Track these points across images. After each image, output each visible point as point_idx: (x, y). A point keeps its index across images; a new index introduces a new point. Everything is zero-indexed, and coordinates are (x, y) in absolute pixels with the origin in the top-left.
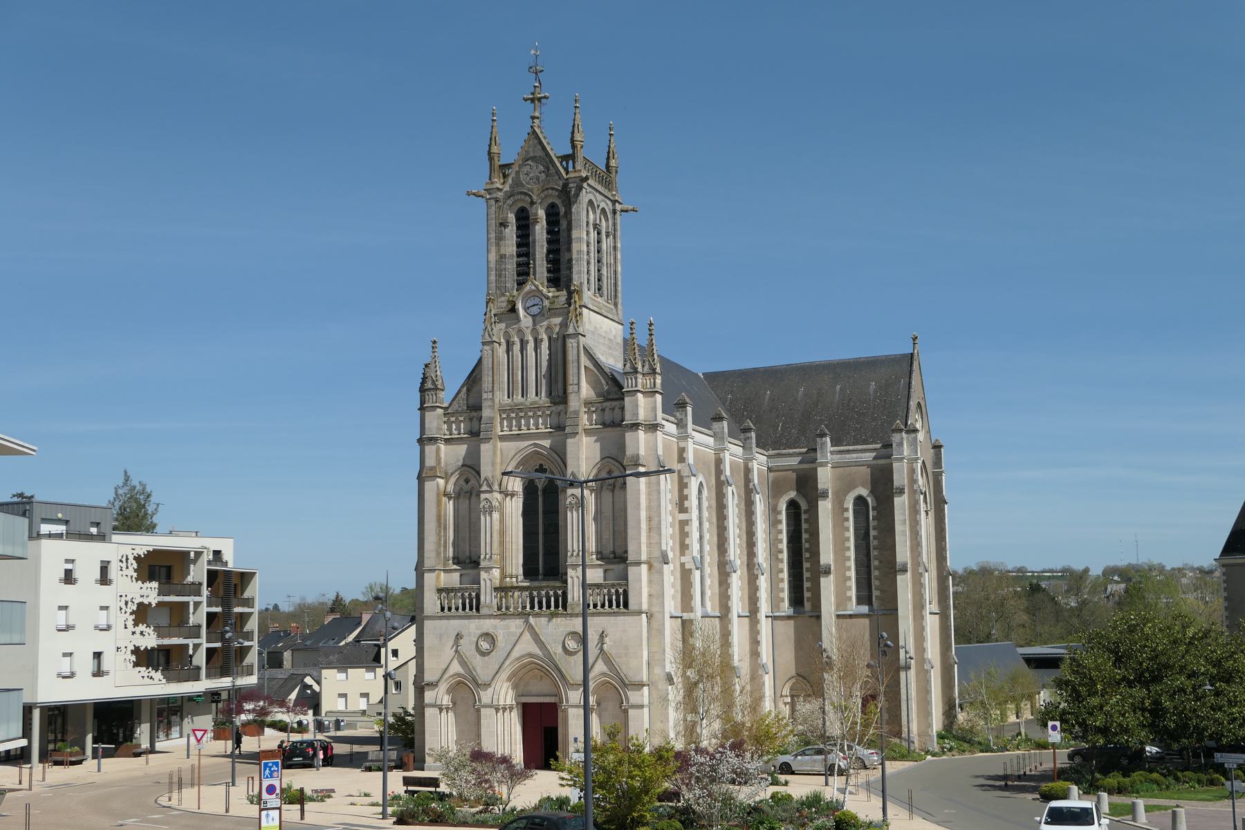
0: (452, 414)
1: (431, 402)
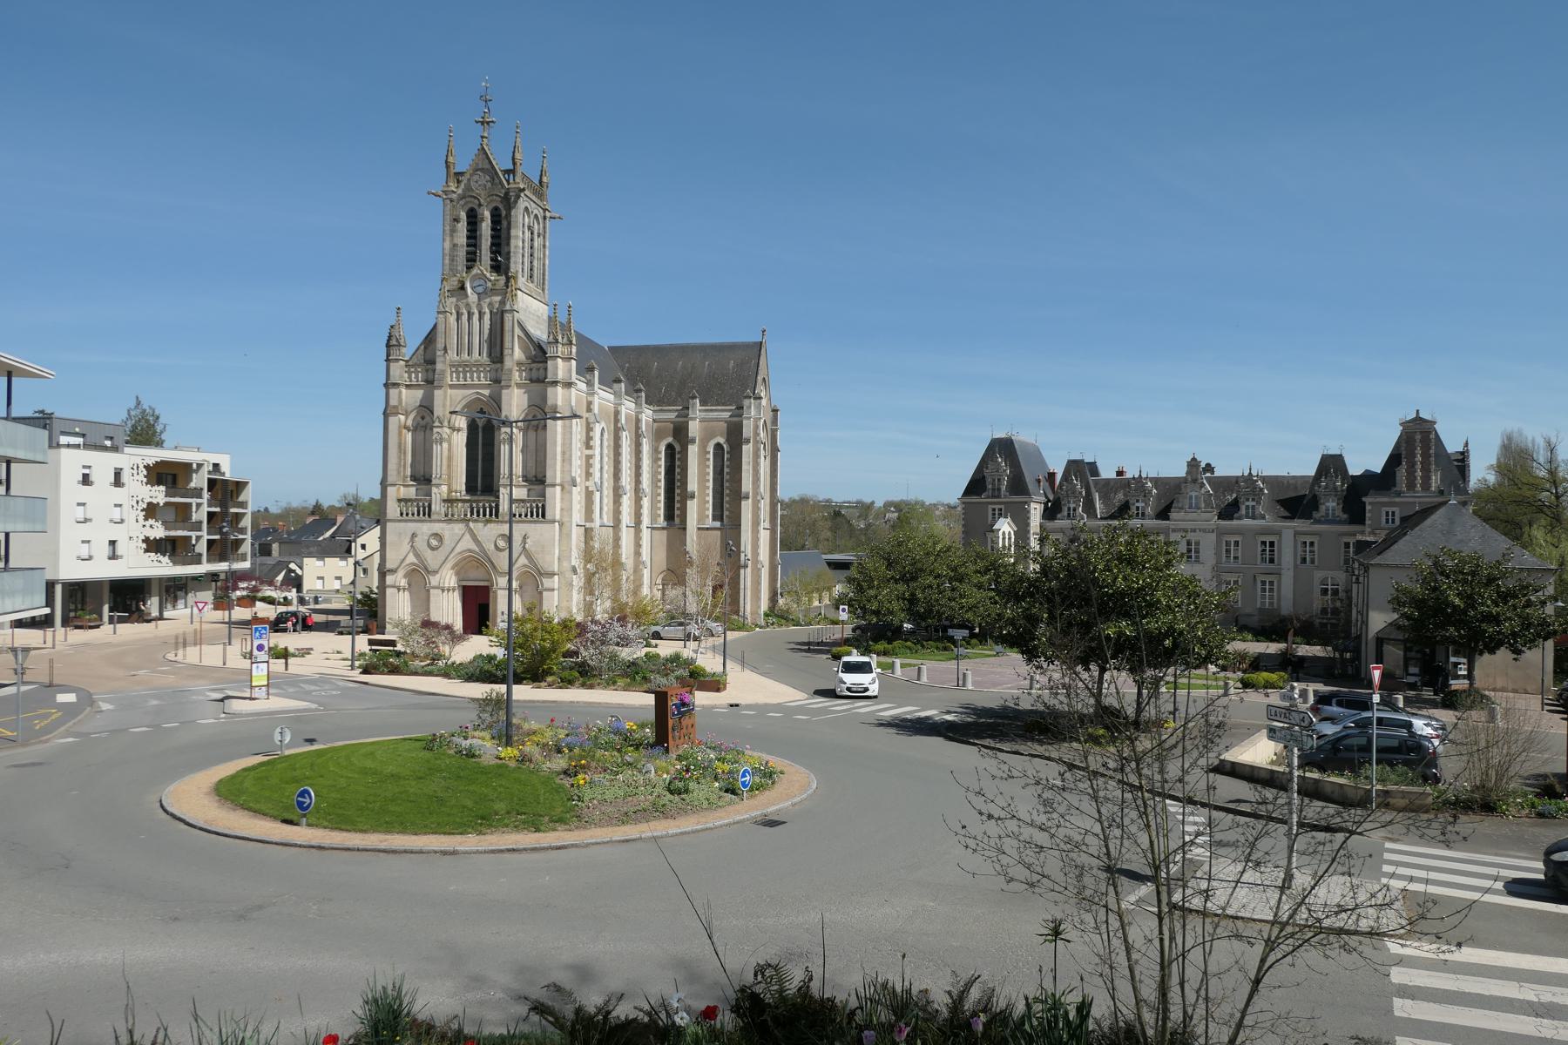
0: (413, 366)
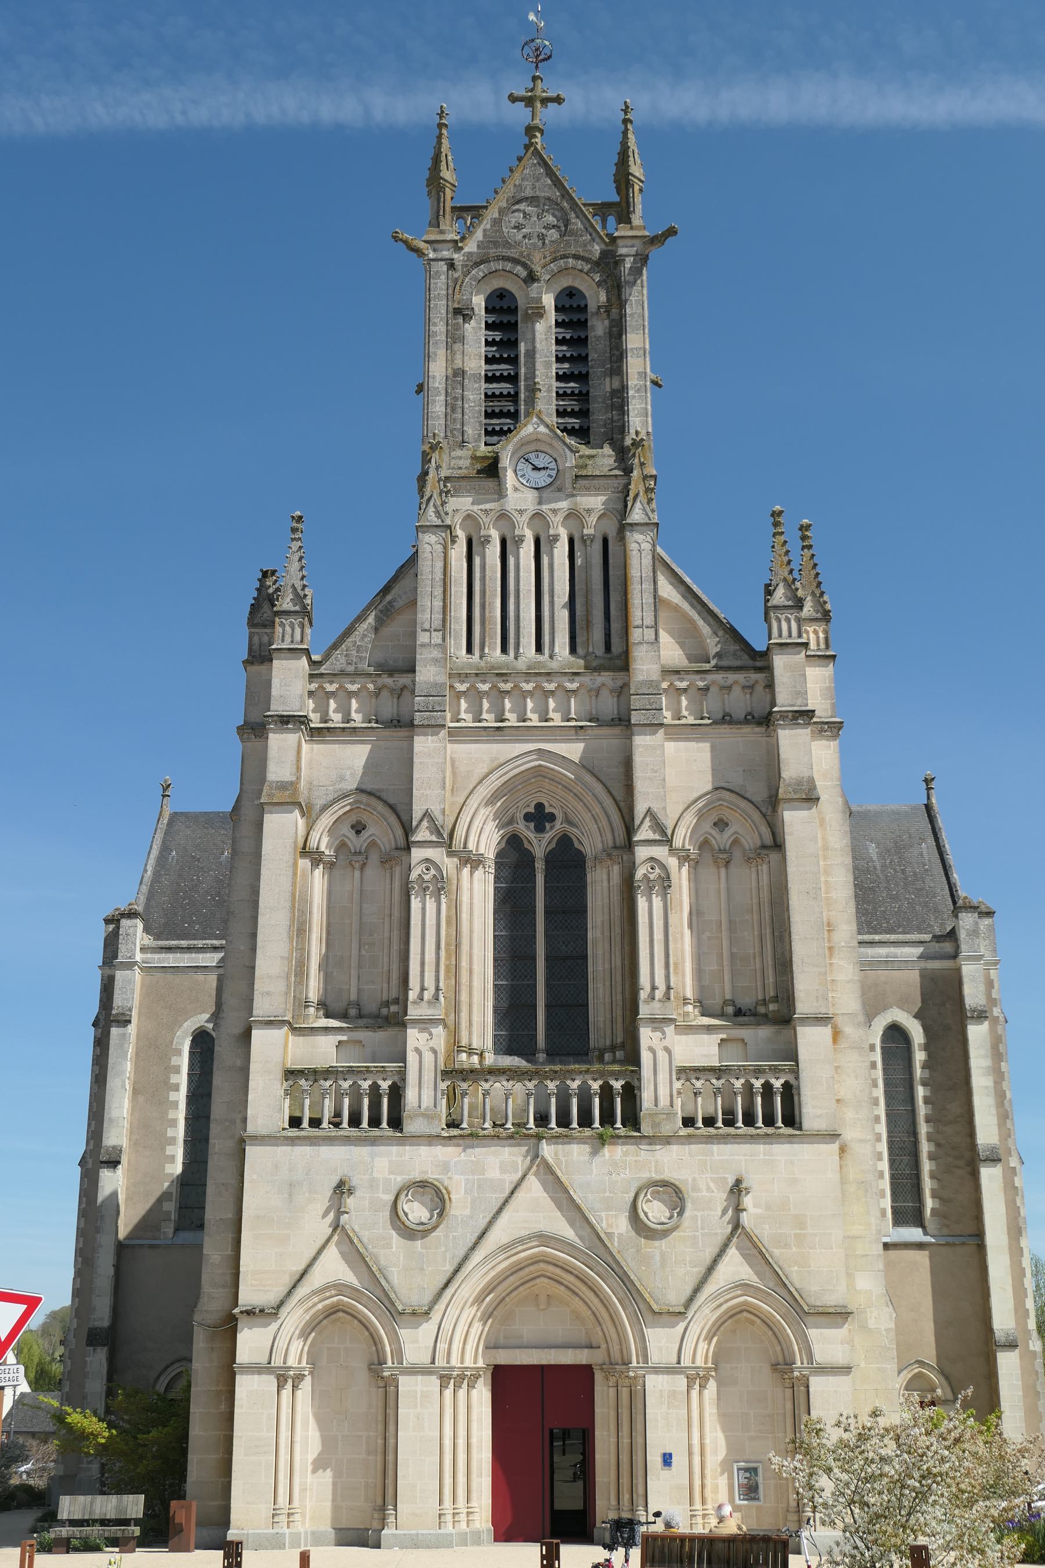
0: (333, 676)
1: (288, 638)
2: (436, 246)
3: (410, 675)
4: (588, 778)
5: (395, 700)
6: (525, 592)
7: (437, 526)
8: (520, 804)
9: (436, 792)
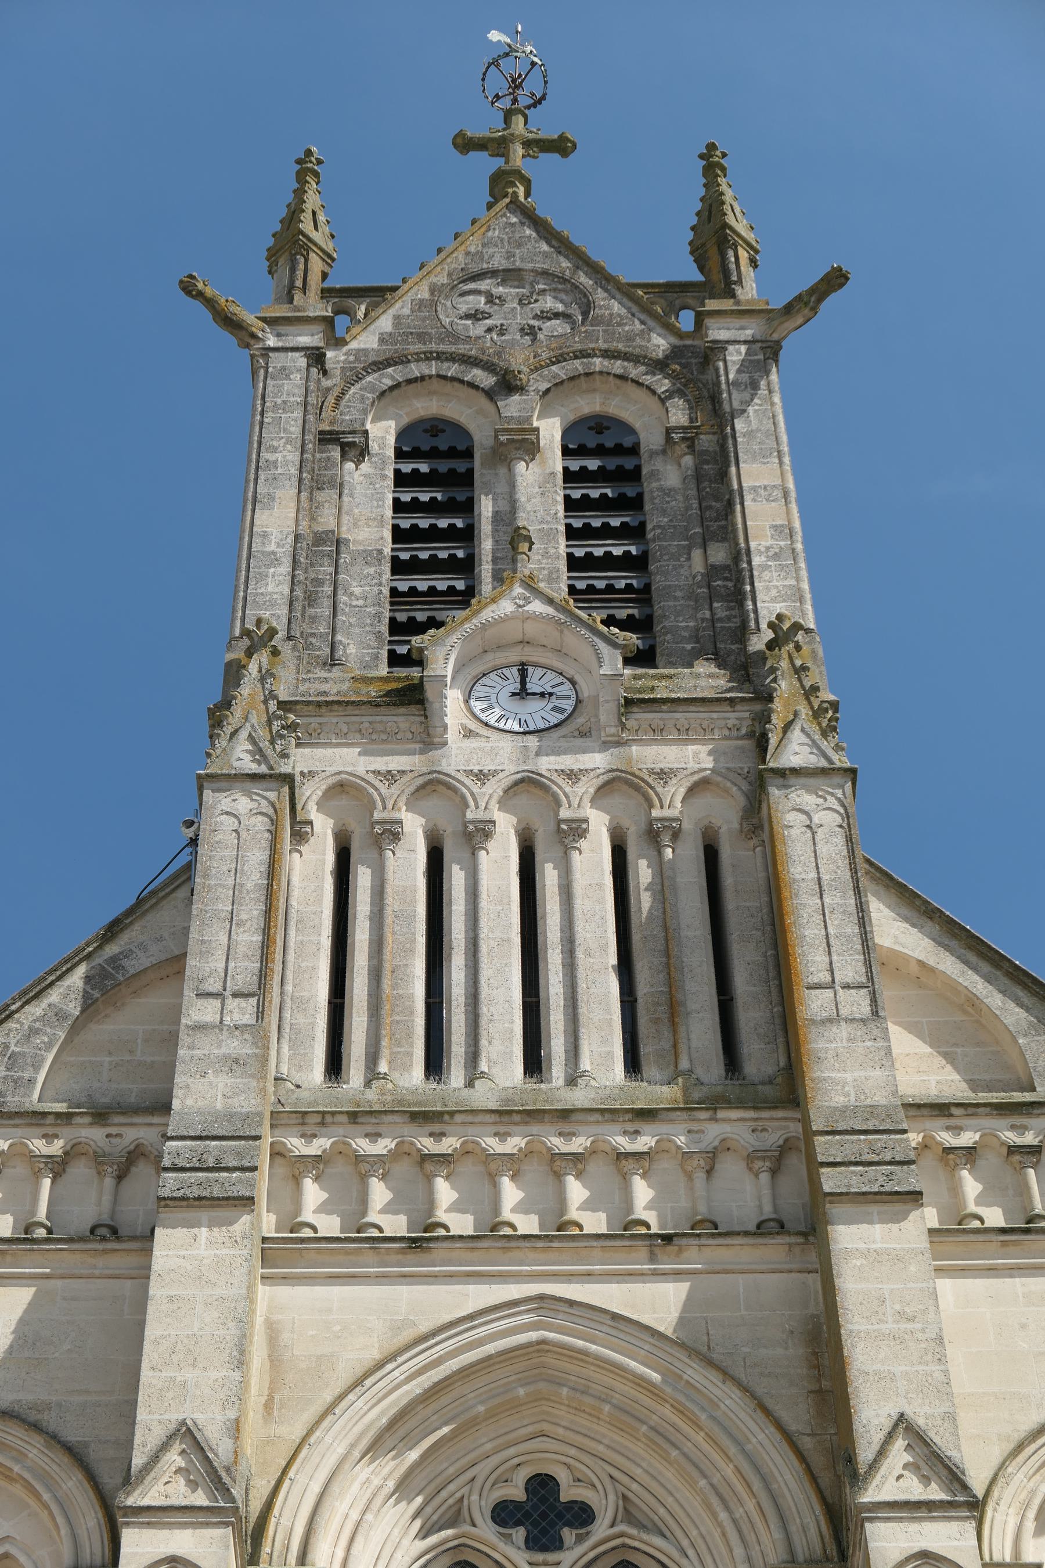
2: (282, 329)
3: (156, 1120)
4: (695, 1373)
5: (109, 1182)
6: (493, 944)
7: (254, 777)
8: (481, 1470)
9: (213, 1375)
